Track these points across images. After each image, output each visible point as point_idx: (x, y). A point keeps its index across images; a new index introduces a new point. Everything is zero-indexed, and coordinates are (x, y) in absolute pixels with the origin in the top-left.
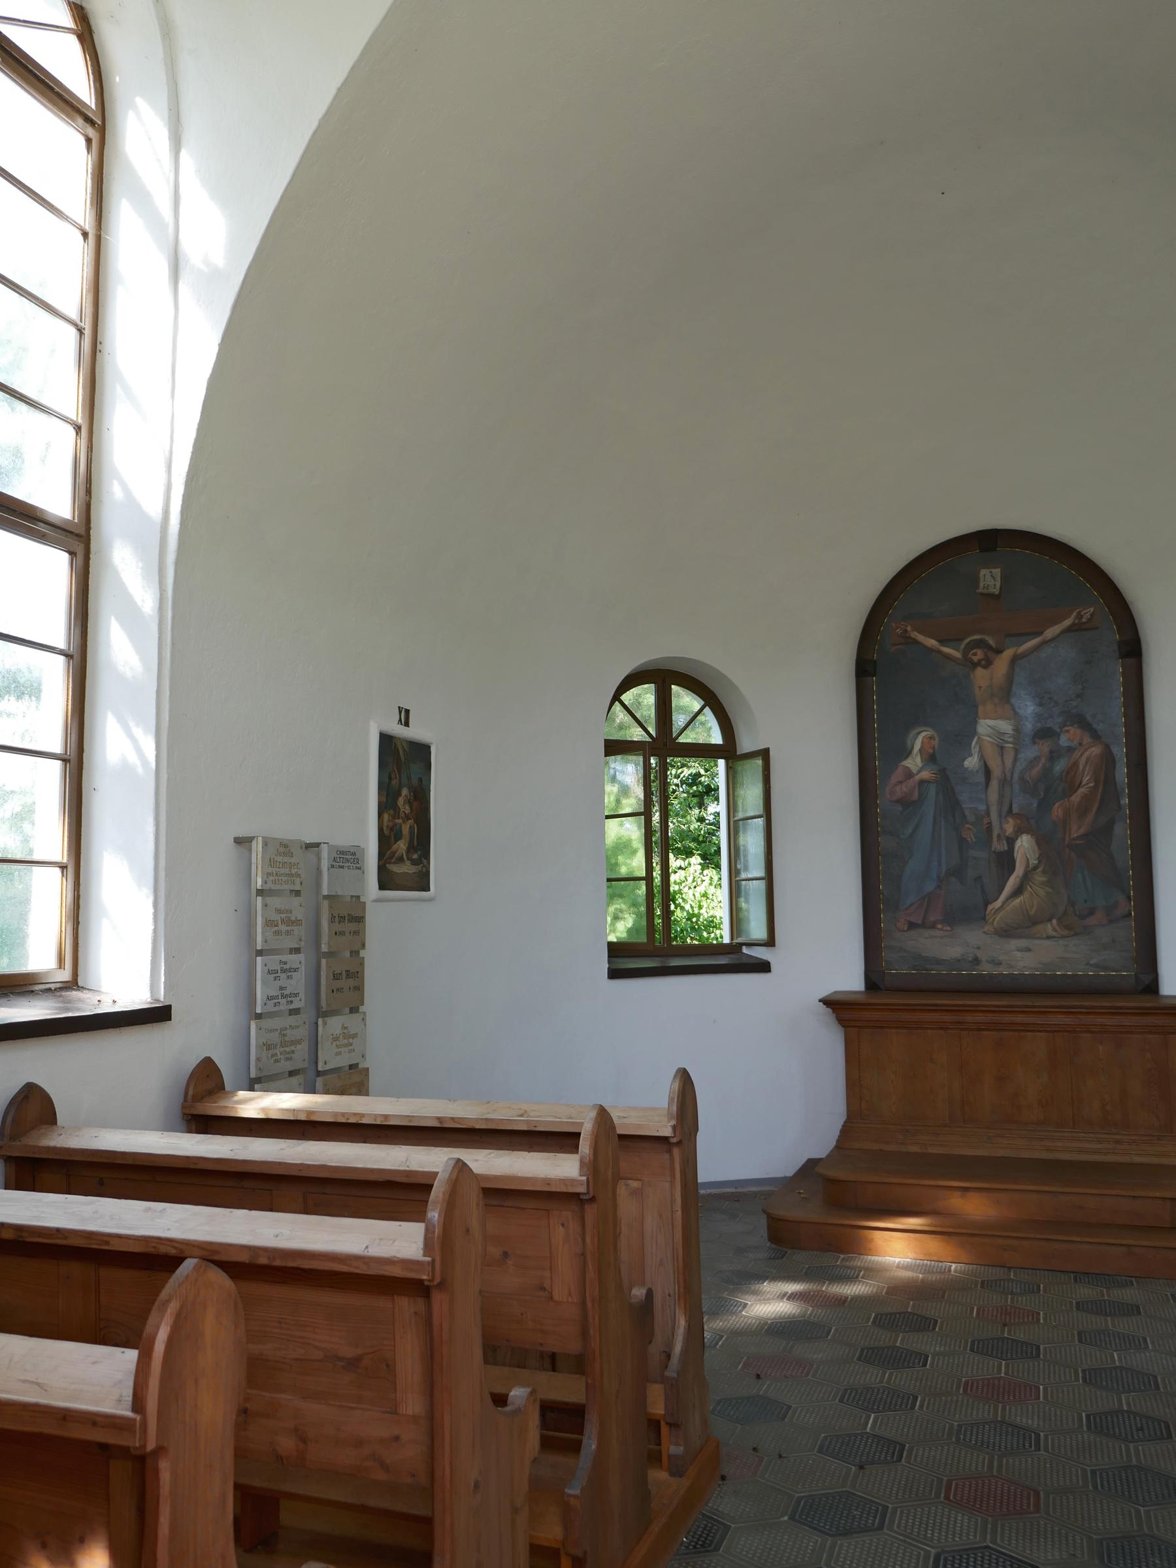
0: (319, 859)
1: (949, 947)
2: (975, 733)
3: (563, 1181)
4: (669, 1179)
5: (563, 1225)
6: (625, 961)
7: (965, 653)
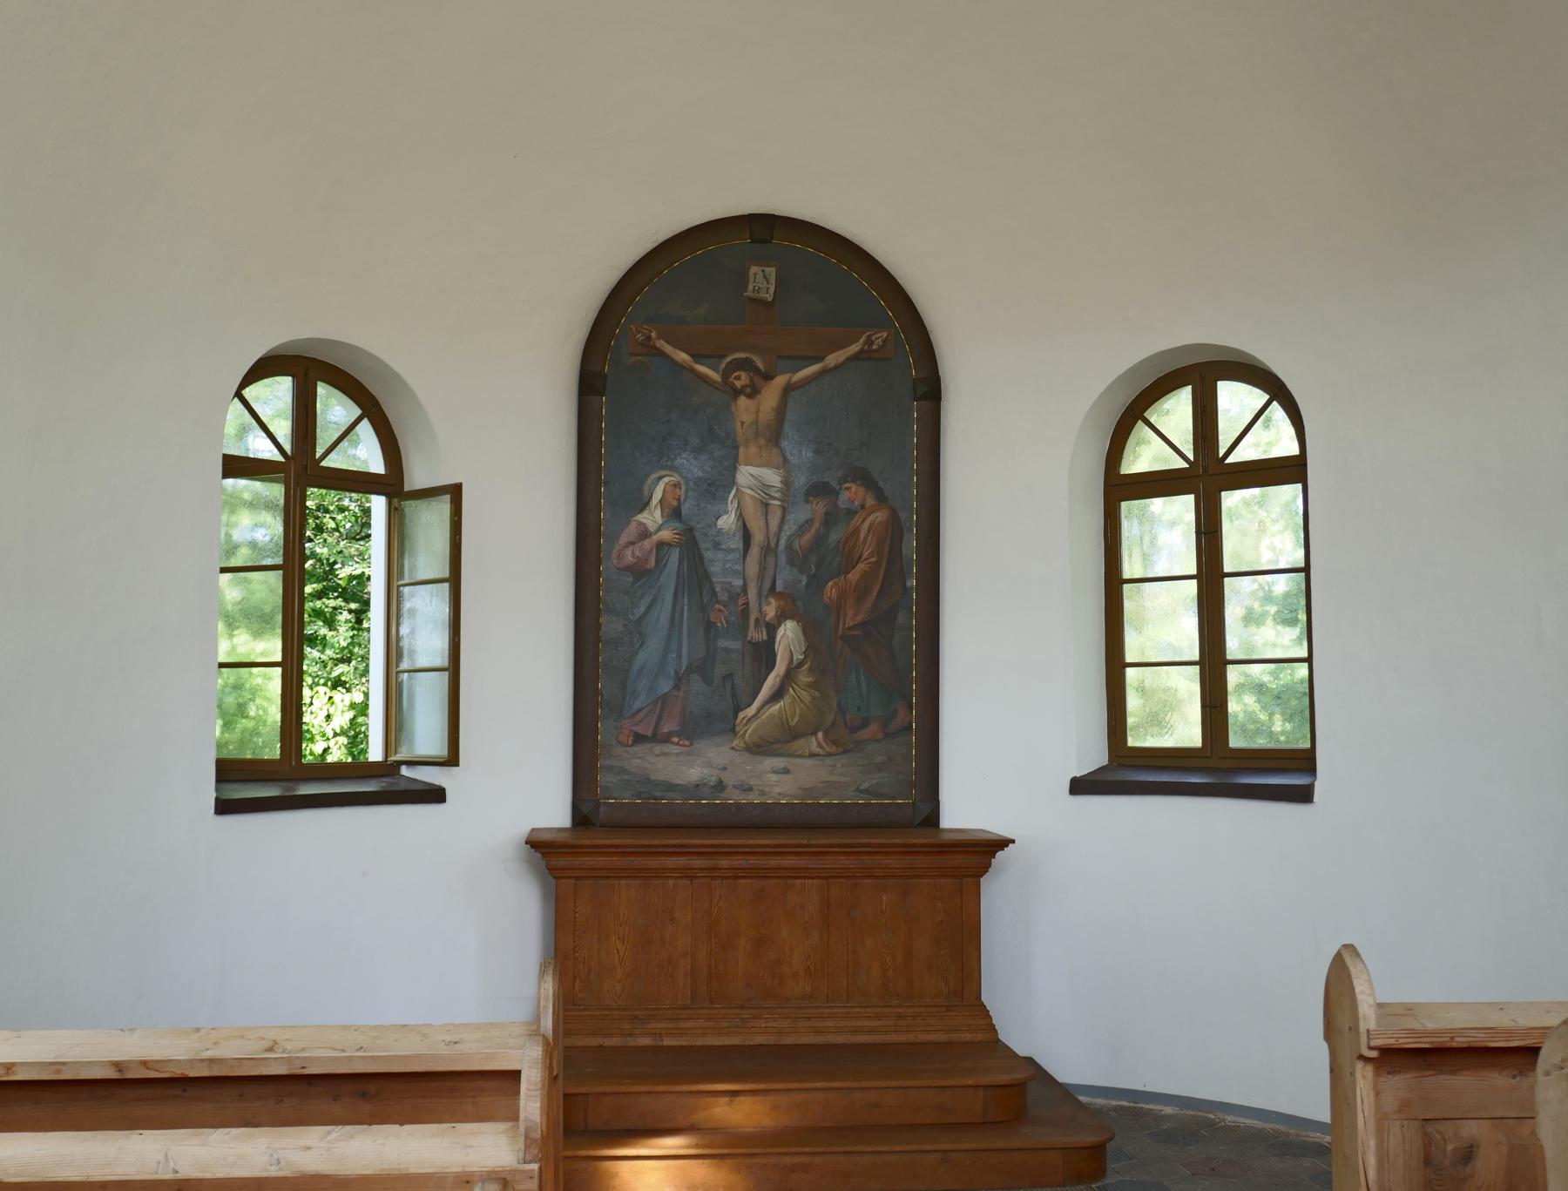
1: (690, 767)
2: (733, 482)
7: (725, 376)
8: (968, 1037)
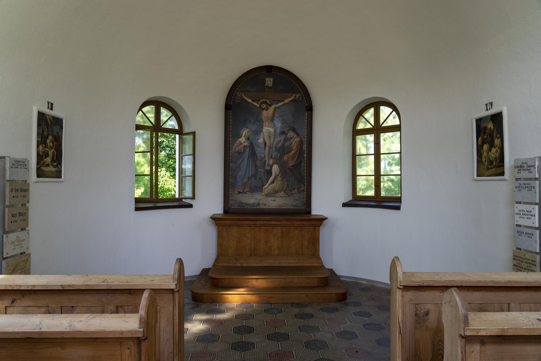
0: (5, 164)
1: (251, 199)
2: (262, 131)
3: (130, 332)
4: (172, 305)
5: (128, 349)
6: (141, 205)
7: (260, 106)
8: (316, 265)
